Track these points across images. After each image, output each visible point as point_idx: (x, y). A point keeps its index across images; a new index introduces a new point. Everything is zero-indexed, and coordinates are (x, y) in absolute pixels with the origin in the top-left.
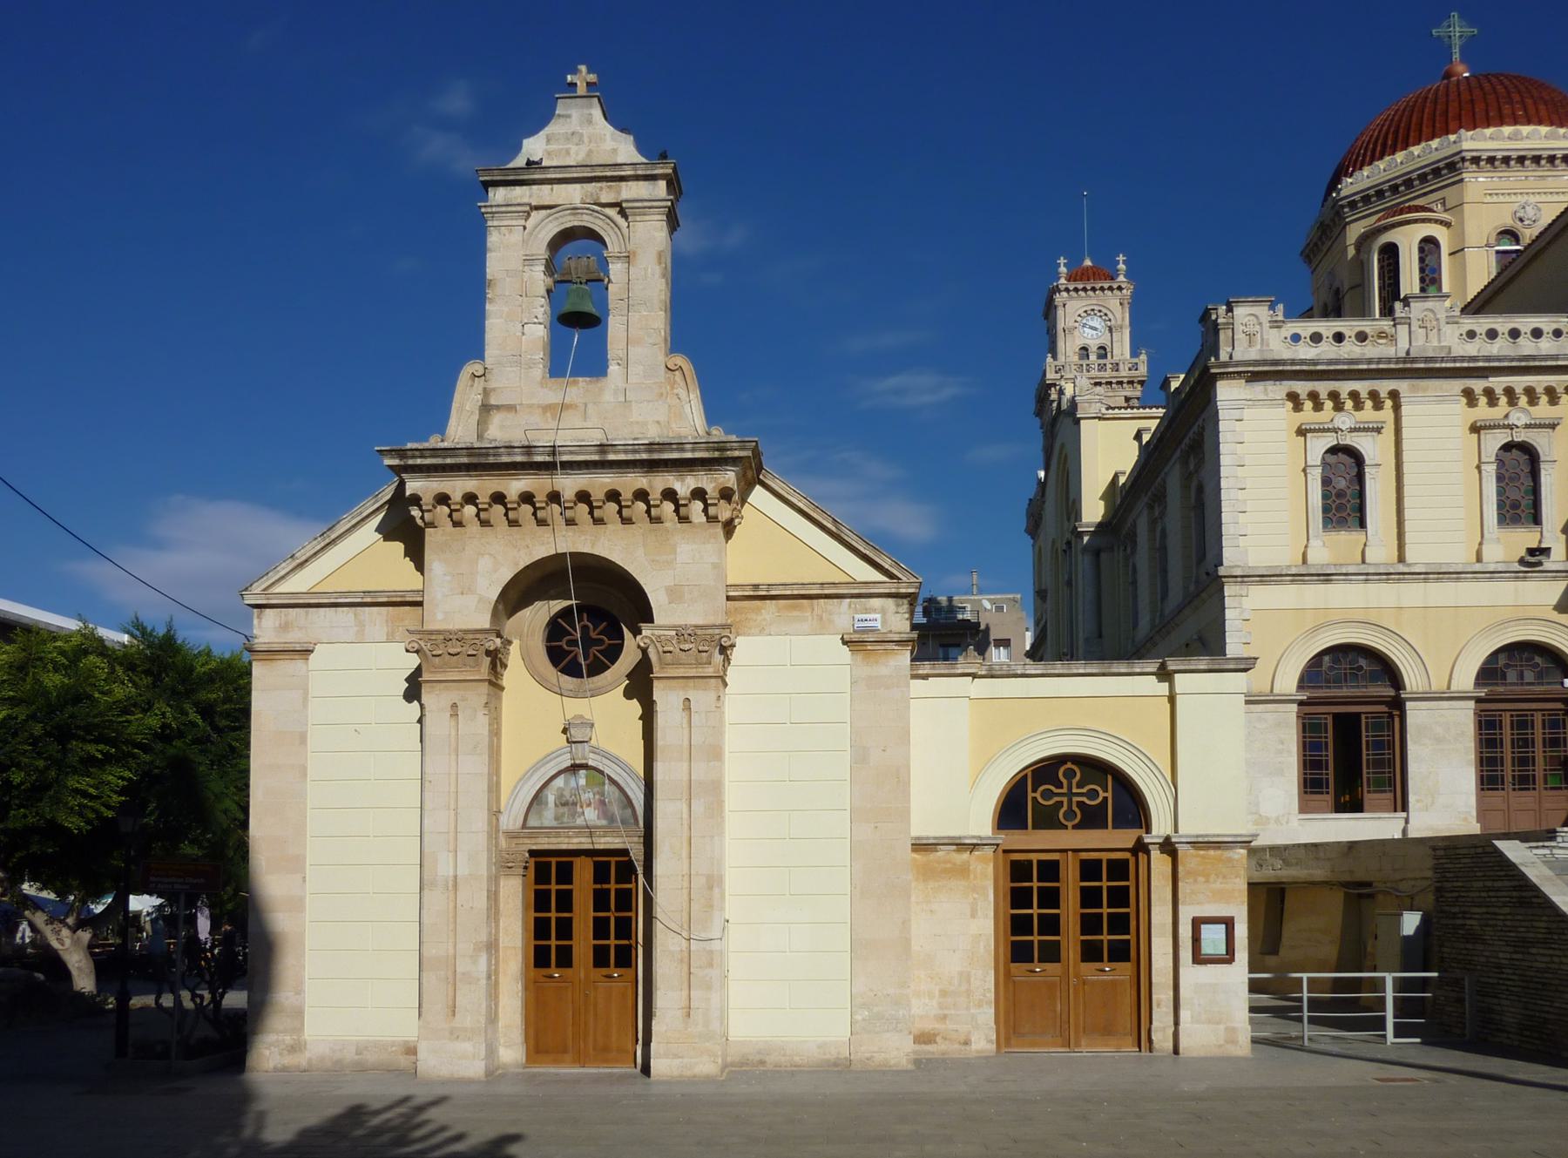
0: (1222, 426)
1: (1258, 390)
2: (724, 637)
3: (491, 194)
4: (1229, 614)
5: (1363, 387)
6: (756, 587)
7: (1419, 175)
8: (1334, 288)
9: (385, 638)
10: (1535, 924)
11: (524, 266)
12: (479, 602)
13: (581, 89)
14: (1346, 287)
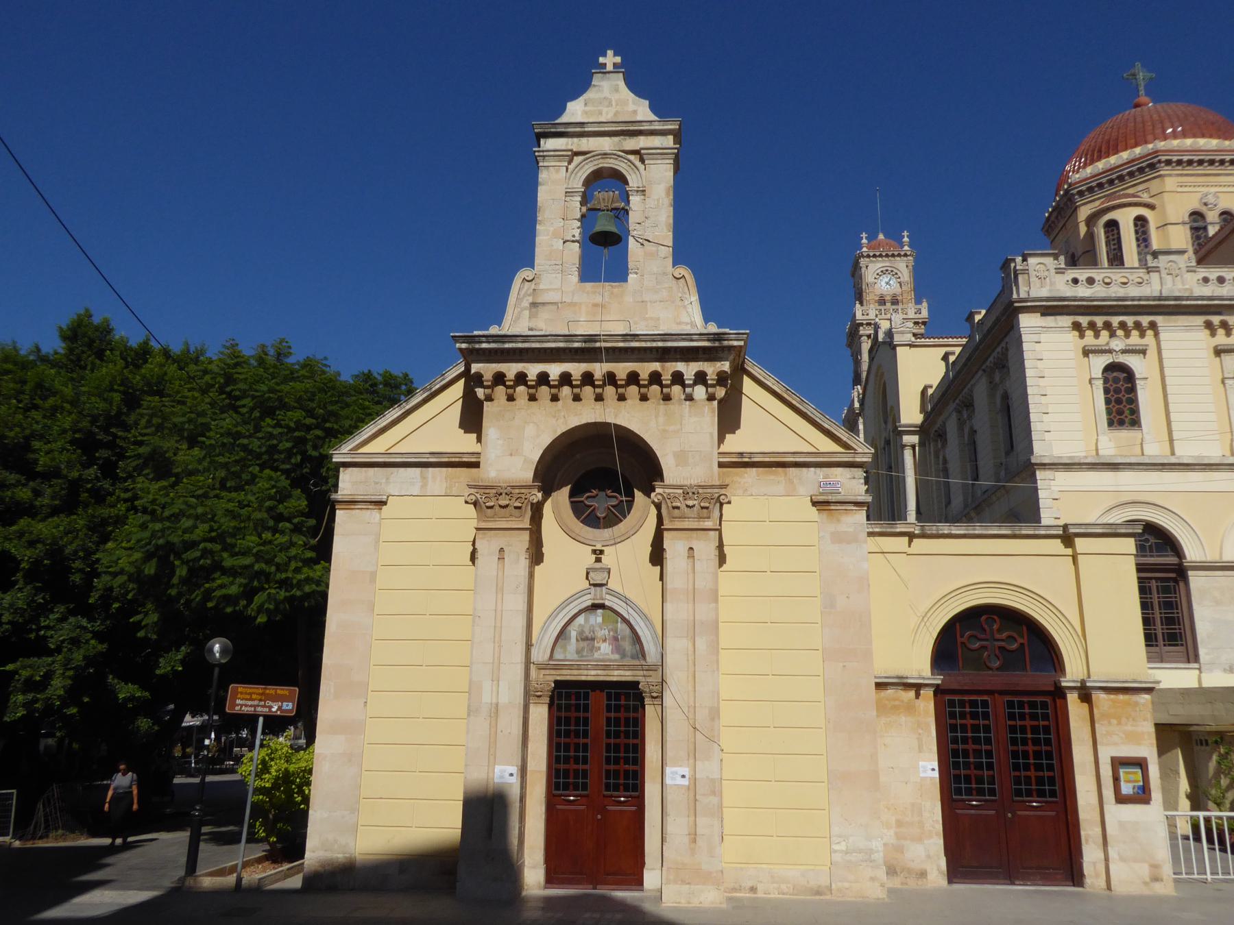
0: (1025, 346)
1: (1050, 321)
3: (542, 141)
4: (1041, 494)
5: (1130, 320)
7: (1108, 180)
8: (1070, 253)
13: (610, 67)
14: (1080, 253)
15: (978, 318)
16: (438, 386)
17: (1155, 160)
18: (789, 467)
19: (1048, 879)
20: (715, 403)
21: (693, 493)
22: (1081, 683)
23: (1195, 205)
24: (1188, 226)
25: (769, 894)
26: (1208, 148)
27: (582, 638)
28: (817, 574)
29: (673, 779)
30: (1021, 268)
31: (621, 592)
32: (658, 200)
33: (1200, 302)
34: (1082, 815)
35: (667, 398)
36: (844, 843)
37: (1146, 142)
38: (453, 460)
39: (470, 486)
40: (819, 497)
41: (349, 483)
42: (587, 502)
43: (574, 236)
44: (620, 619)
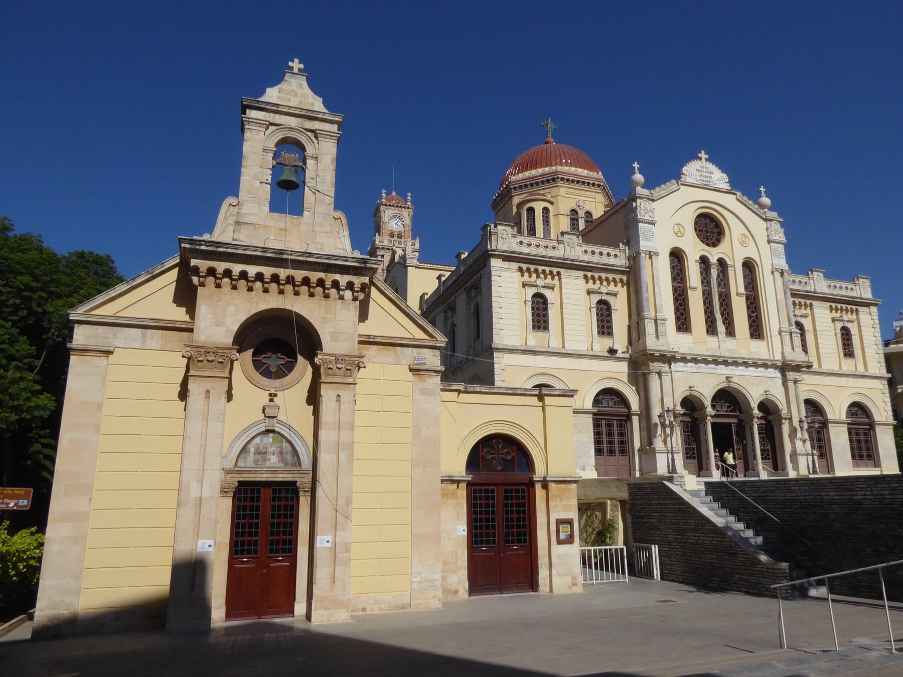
0: (493, 278)
1: (507, 264)
2: (359, 362)
3: (248, 111)
4: (496, 366)
6: (369, 336)
10: (688, 521)
12: (226, 331)
13: (296, 70)
15: (463, 256)
16: (158, 271)
17: (556, 177)
18: (397, 346)
19: (520, 589)
20: (358, 302)
21: (342, 360)
22: (543, 479)
23: (573, 206)
24: (569, 217)
25: (373, 611)
26: (583, 174)
27: (258, 452)
28: (411, 413)
29: (321, 543)
30: (494, 231)
31: (286, 422)
32: (326, 165)
33: (582, 264)
34: (540, 552)
35: (327, 296)
36: (419, 577)
37: (551, 165)
38: (168, 325)
39: (186, 346)
40: (414, 366)
41: (81, 336)
42: (263, 361)
43: (267, 180)
44: (284, 440)
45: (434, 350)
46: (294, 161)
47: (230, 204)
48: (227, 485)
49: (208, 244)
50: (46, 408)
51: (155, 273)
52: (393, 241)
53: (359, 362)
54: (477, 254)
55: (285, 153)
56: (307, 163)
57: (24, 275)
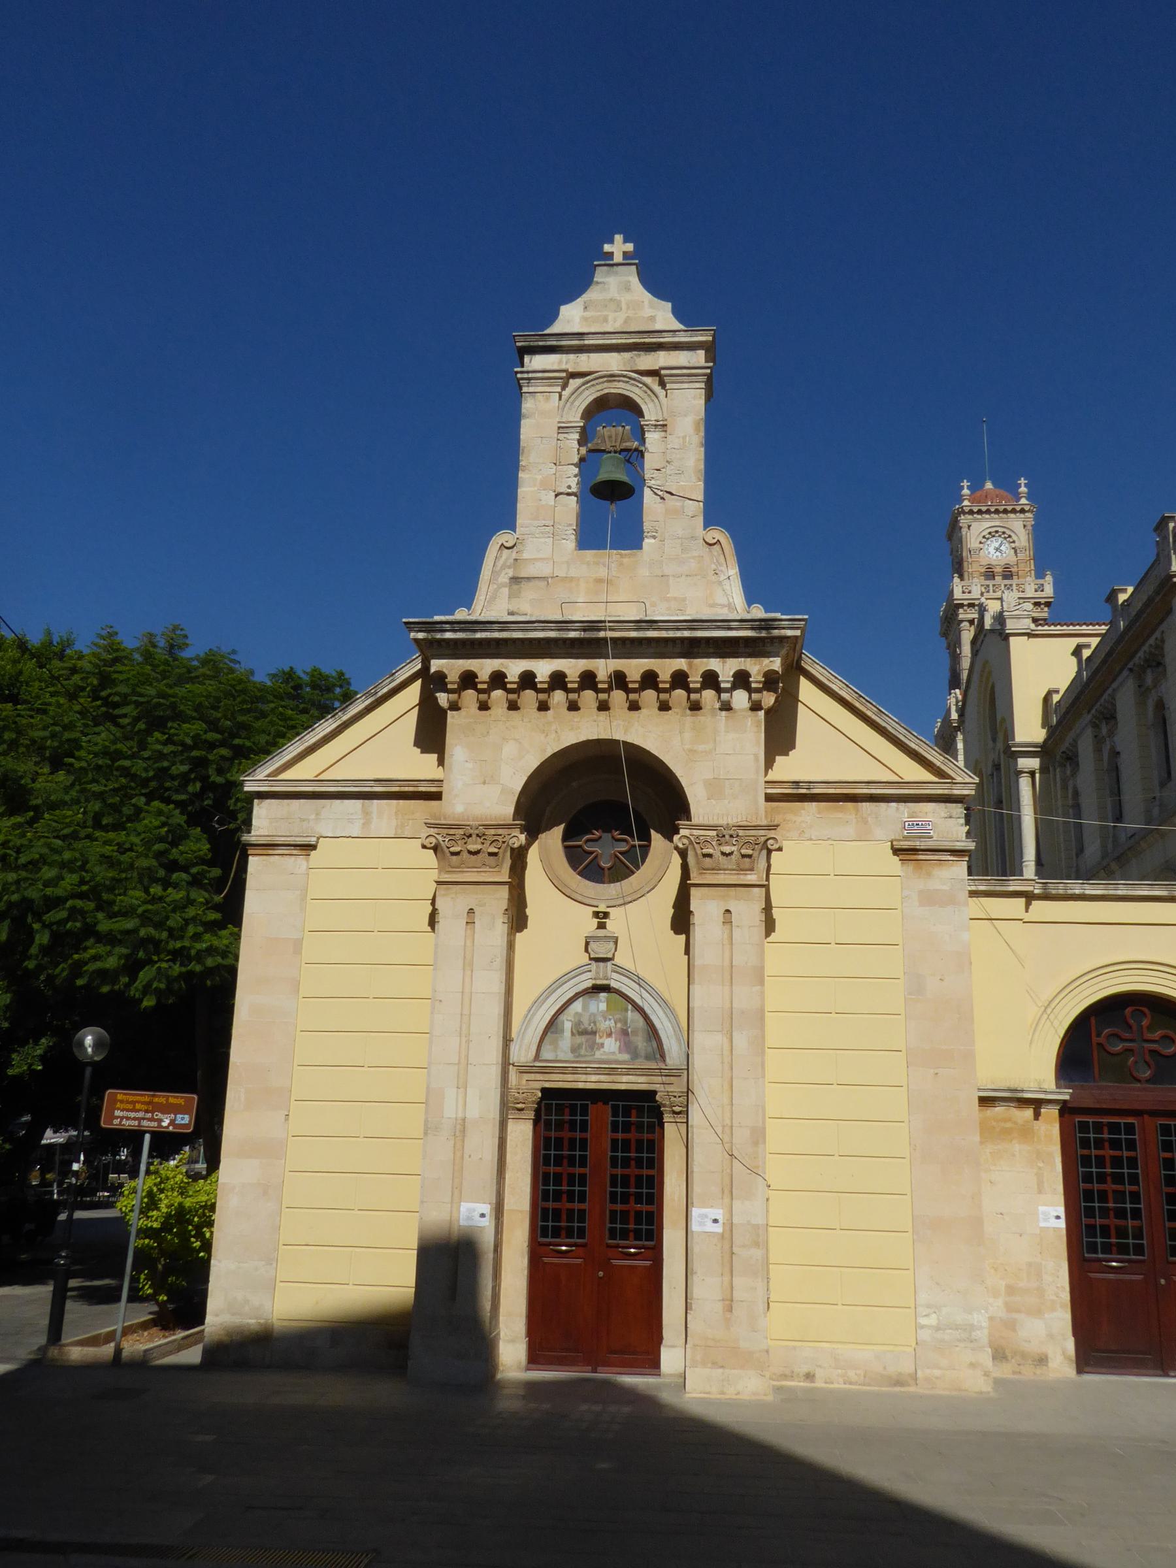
2: (768, 840)
3: (527, 359)
9: (394, 832)
11: (559, 433)
13: (618, 258)
16: (385, 690)
18: (862, 801)
20: (762, 713)
21: (731, 836)
29: (701, 1224)
31: (632, 969)
36: (934, 1316)
38: (406, 789)
40: (902, 843)
44: (630, 1006)
45: (948, 805)
46: (623, 441)
47: (502, 544)
48: (521, 1096)
49: (457, 627)
50: (228, 952)
51: (380, 694)
52: (994, 585)
53: (768, 840)
54: (1150, 588)
55: (604, 427)
56: (647, 440)
57: (194, 721)
